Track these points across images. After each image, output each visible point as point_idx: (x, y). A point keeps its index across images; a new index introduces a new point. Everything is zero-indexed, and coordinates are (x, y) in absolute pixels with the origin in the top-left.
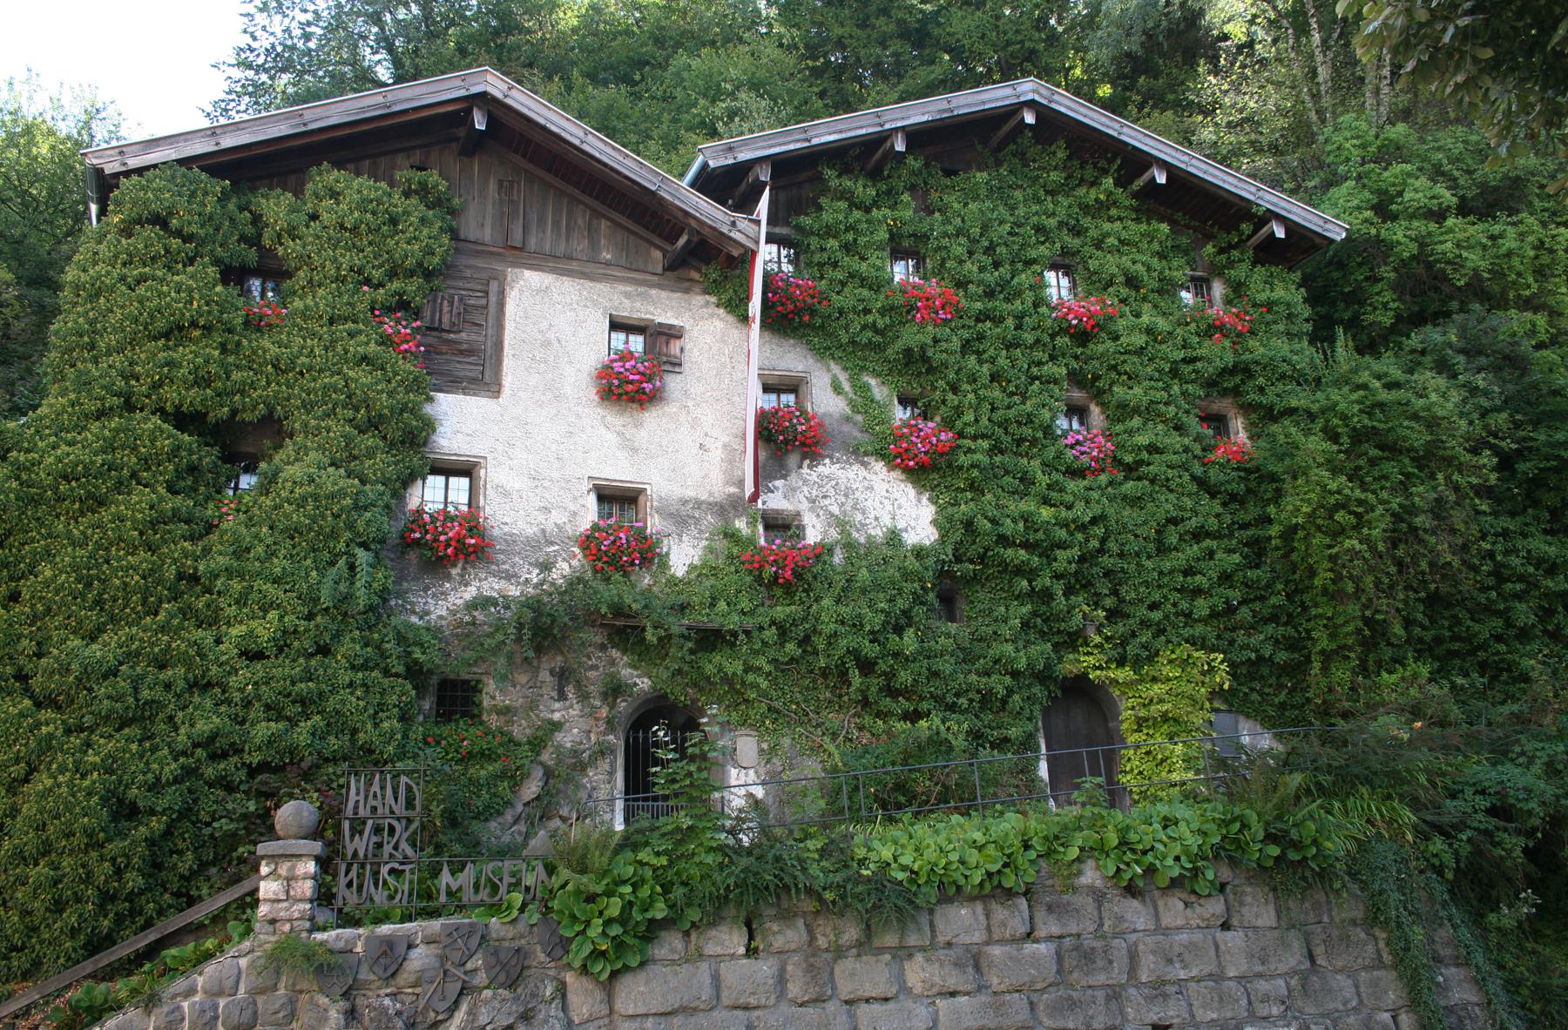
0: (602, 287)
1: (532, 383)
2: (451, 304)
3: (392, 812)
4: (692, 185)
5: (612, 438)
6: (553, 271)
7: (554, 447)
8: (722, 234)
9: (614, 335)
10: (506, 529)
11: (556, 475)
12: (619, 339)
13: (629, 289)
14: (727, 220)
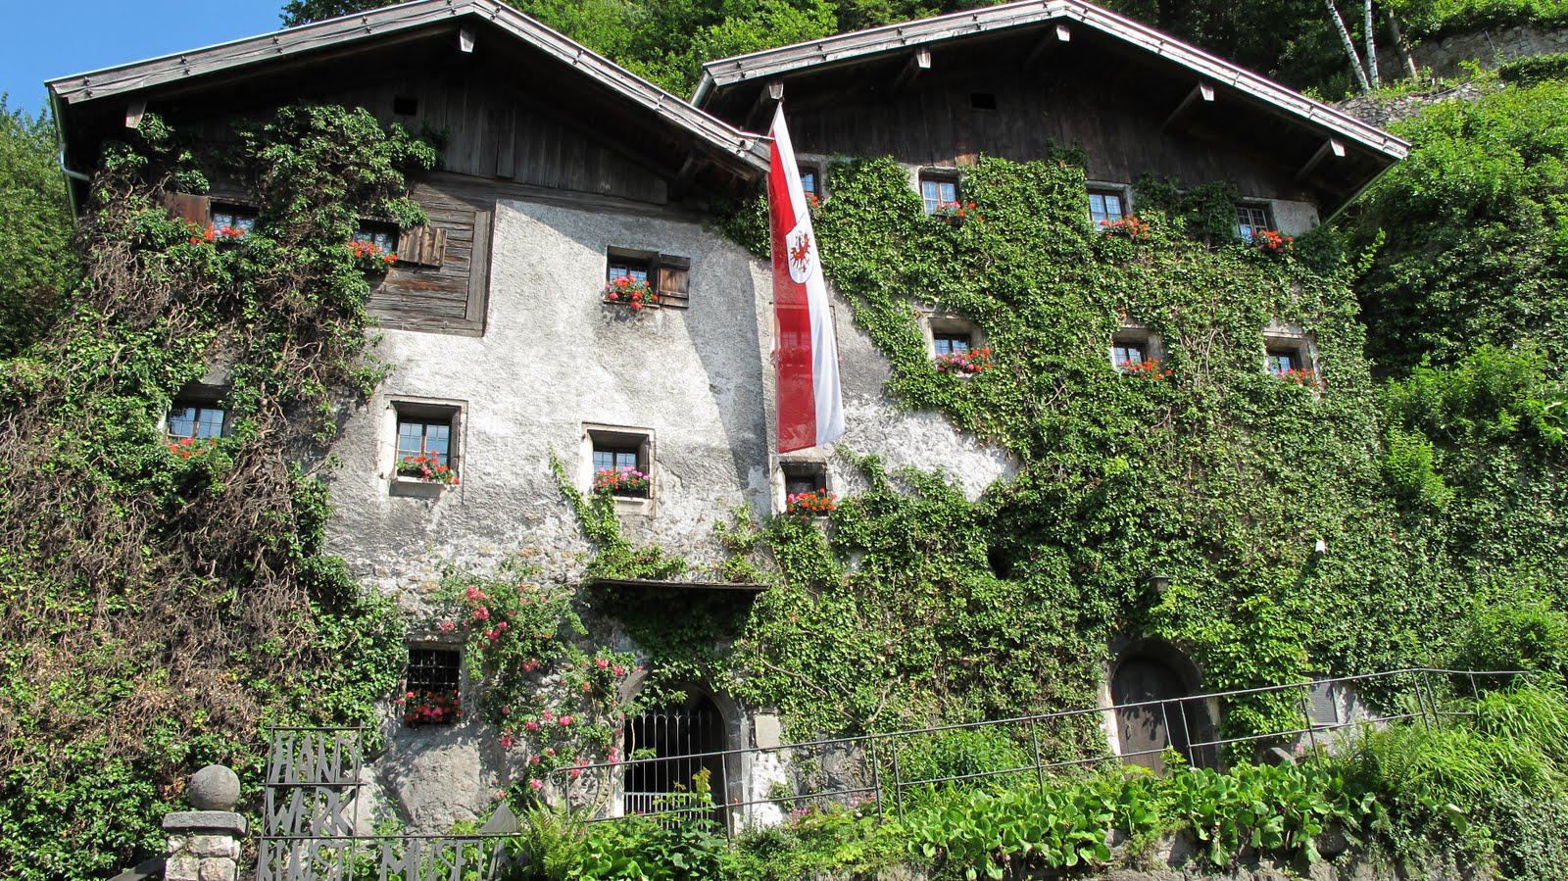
0: (600, 218)
1: (521, 319)
2: (433, 236)
3: (324, 779)
4: (701, 105)
5: (609, 379)
6: (546, 201)
7: (544, 390)
8: (731, 155)
9: (613, 271)
10: (489, 480)
11: (545, 420)
12: (620, 274)
13: (630, 219)
14: (737, 141)
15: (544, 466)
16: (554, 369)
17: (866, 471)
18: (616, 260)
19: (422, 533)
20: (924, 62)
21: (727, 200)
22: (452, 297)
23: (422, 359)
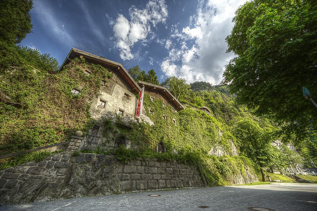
5: (122, 104)
15: (114, 110)
16: (117, 101)
17: (143, 120)
18: (125, 94)
19: (100, 113)
20: (155, 88)
21: (135, 92)
22: (109, 90)
23: (105, 96)
